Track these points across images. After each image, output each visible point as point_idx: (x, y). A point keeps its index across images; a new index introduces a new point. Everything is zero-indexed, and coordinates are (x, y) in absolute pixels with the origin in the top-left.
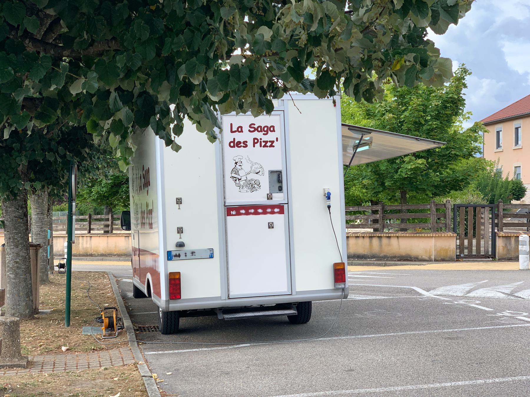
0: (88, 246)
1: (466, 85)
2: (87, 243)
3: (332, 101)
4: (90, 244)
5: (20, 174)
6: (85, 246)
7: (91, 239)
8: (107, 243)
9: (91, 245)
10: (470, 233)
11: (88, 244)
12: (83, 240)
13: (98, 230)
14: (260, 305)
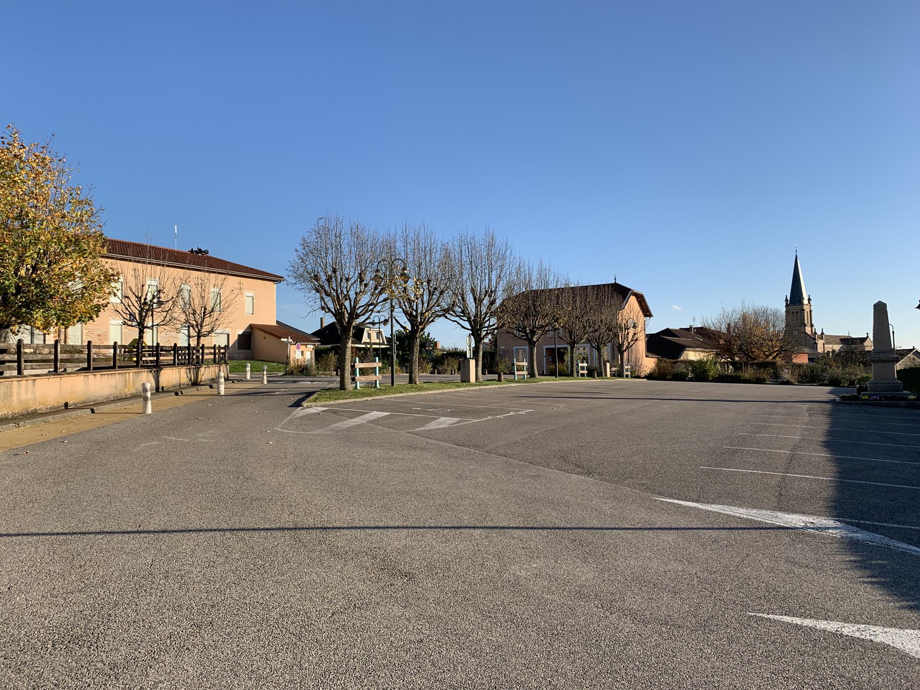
0: (30, 396)
1: (435, 340)
2: (27, 392)
3: (113, 311)
4: (32, 392)
5: (371, 337)
6: (23, 397)
7: (34, 385)
8: (60, 388)
9: (35, 394)
10: (348, 373)
11: (30, 392)
12: (19, 386)
13: (32, 369)
14: (846, 341)
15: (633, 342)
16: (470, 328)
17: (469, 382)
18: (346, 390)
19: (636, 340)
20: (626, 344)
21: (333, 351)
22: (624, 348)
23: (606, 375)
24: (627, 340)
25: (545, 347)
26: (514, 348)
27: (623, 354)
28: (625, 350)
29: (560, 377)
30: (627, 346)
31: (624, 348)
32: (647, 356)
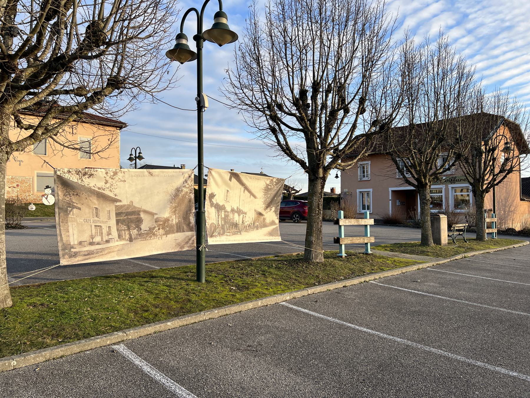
15: (504, 174)
16: (301, 128)
17: (374, 220)
18: (167, 54)
19: (510, 171)
20: (488, 178)
21: (278, 239)
22: (485, 187)
23: (438, 241)
24: (492, 170)
25: (391, 189)
26: (358, 191)
27: (482, 198)
28: (487, 191)
29: (467, 234)
30: (489, 183)
31: (485, 187)
32: (521, 200)
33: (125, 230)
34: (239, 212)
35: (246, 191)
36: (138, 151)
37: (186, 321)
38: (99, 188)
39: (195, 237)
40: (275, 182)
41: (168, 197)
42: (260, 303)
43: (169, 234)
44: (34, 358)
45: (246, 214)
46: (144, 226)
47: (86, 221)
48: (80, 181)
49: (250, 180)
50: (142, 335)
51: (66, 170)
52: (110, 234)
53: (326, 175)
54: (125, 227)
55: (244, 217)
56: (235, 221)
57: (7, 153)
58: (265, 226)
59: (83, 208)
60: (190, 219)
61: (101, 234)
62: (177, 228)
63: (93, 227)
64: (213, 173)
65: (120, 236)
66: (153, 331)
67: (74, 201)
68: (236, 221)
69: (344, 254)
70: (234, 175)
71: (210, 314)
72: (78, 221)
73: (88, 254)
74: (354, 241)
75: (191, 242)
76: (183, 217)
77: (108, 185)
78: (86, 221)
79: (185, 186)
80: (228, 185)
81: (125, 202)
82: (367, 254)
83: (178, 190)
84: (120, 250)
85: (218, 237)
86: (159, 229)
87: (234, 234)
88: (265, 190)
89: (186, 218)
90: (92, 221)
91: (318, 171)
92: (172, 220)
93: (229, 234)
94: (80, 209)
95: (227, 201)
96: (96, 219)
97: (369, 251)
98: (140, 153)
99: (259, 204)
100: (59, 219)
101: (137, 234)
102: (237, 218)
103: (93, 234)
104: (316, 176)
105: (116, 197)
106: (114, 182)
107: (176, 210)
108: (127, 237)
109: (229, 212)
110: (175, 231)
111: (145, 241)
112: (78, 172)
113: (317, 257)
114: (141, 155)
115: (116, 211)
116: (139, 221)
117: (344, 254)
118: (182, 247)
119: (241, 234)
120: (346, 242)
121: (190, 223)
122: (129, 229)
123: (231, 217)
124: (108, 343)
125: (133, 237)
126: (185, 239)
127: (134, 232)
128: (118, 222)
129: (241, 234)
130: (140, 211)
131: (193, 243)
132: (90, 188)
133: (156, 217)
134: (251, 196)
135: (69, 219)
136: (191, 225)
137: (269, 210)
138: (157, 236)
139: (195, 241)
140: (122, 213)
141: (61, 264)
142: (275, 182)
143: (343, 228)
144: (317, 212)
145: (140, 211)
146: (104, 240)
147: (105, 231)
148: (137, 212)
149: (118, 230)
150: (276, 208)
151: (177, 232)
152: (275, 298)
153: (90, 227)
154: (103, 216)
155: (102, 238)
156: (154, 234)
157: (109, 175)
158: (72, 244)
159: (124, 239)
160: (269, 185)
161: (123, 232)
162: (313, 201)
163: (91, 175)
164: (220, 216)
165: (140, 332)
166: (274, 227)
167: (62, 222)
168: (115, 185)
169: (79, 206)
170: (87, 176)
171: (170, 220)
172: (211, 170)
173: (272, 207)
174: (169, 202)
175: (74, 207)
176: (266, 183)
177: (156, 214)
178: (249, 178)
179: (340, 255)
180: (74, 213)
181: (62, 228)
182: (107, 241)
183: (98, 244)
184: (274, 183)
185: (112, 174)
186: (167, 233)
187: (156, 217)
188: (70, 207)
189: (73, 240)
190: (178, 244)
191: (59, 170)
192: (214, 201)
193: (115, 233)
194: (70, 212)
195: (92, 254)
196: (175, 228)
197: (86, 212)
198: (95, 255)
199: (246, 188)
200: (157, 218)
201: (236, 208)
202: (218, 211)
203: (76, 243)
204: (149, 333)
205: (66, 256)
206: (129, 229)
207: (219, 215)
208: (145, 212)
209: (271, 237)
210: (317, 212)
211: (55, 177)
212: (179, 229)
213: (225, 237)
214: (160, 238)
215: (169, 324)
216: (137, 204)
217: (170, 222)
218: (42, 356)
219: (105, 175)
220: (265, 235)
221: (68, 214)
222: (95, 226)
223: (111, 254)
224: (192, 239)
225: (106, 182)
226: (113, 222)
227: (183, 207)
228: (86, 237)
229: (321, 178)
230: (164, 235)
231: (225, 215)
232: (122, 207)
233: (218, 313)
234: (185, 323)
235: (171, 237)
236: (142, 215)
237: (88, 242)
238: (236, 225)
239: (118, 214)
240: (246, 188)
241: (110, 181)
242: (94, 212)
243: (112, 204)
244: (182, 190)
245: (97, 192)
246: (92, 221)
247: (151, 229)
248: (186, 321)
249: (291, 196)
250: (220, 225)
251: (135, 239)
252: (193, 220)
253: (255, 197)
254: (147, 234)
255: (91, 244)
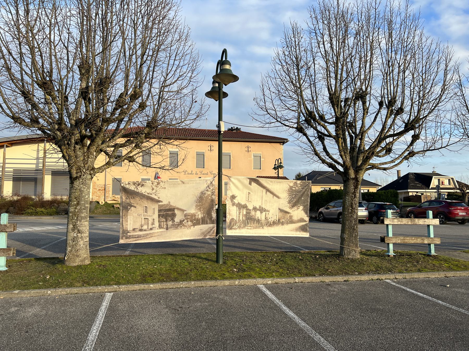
33: (163, 222)
34: (262, 210)
35: (268, 193)
36: (279, 162)
37: (166, 286)
38: (148, 194)
39: (215, 228)
40: (300, 184)
41: (195, 198)
42: (237, 283)
43: (196, 225)
44: (60, 292)
45: (268, 211)
46: (177, 220)
47: (139, 215)
48: (136, 189)
49: (271, 183)
50: (130, 290)
51: (127, 183)
52: (154, 224)
53: (358, 176)
54: (164, 220)
55: (267, 214)
56: (257, 218)
57: (91, 174)
58: (292, 222)
59: (137, 206)
60: (211, 215)
61: (148, 224)
62: (202, 221)
63: (143, 219)
64: (232, 179)
65: (160, 227)
66: (138, 288)
67: (132, 202)
68: (258, 217)
69: (392, 253)
70: (252, 180)
71: (186, 284)
72: (134, 215)
73: (138, 237)
74: (406, 241)
75: (212, 232)
76: (207, 213)
77: (154, 191)
78: (139, 215)
79: (207, 190)
80: (249, 189)
81: (165, 202)
82: (429, 255)
83: (203, 193)
84: (160, 235)
85: (238, 230)
86: (188, 221)
87: (256, 228)
88: (289, 191)
89: (209, 213)
90: (142, 215)
91: (348, 173)
92: (198, 215)
93: (250, 228)
94: (135, 207)
95: (248, 201)
96: (146, 214)
97: (433, 252)
98: (280, 163)
99: (284, 203)
100: (122, 213)
101: (171, 225)
102: (258, 215)
103: (143, 223)
104: (347, 177)
105: (159, 199)
106: (158, 189)
107: (201, 208)
108: (165, 226)
109: (250, 210)
110: (201, 224)
111: (177, 230)
112: (134, 184)
113: (349, 253)
114: (281, 164)
115: (158, 208)
116: (174, 215)
117: (392, 253)
118: (205, 236)
119: (263, 228)
120: (394, 241)
121: (212, 217)
122: (166, 221)
123: (253, 214)
124: (106, 291)
125: (169, 227)
126: (208, 230)
127: (170, 223)
128: (159, 216)
129: (263, 228)
130: (174, 209)
131: (213, 233)
132: (142, 194)
133: (185, 212)
134: (274, 197)
135: (129, 214)
136: (213, 219)
137: (296, 209)
138: (186, 227)
139: (215, 231)
140: (162, 210)
141: (119, 243)
142: (300, 184)
143: (390, 228)
144: (350, 211)
145: (174, 209)
146: (149, 228)
147: (150, 222)
148: (172, 210)
149: (159, 221)
150: (304, 207)
151: (202, 224)
152: (255, 280)
153: (141, 219)
154: (150, 212)
155: (148, 227)
156: (184, 225)
157: (154, 184)
158: (129, 230)
159: (162, 228)
160: (293, 187)
161: (163, 223)
162: (346, 200)
163: (143, 185)
164: (241, 213)
165: (129, 288)
166: (304, 223)
167: (124, 216)
168: (159, 191)
169: (135, 205)
170: (140, 186)
171: (196, 215)
172: (230, 177)
173: (300, 206)
174: (195, 202)
175: (131, 206)
176: (289, 186)
177: (186, 211)
178: (270, 182)
179: (388, 254)
180: (132, 209)
181: (123, 220)
182: (151, 229)
183: (145, 230)
184: (299, 185)
185: (156, 184)
186: (194, 225)
187: (185, 212)
188: (129, 206)
189: (130, 228)
190: (203, 233)
191: (123, 183)
192: (236, 201)
193: (157, 224)
194: (129, 209)
195: (140, 237)
196: (201, 221)
197: (140, 209)
198: (141, 238)
199: (268, 190)
200: (186, 214)
201: (258, 207)
202: (240, 209)
203: (131, 229)
204: (135, 289)
205: (124, 238)
206: (166, 221)
207: (240, 213)
208: (178, 209)
209: (298, 233)
210: (350, 211)
211: (121, 188)
212: (203, 221)
213: (246, 230)
214: (189, 228)
215: (152, 286)
216: (173, 204)
217: (197, 217)
218: (65, 291)
219: (152, 185)
220: (292, 231)
221: (128, 211)
222: (145, 218)
223: (152, 238)
224: (213, 230)
225: (153, 189)
226: (156, 216)
227: (207, 205)
228: (138, 226)
229: (353, 179)
230: (192, 226)
231: (246, 212)
232: (162, 206)
233: (195, 284)
234: (165, 287)
235: (198, 227)
236: (176, 211)
237: (139, 229)
238: (258, 221)
239: (160, 211)
240: (268, 190)
241: (155, 188)
242: (145, 209)
243: (156, 204)
244: (205, 193)
245: (147, 196)
246: (142, 215)
247: (181, 222)
248: (166, 286)
249: (465, 195)
250: (241, 220)
251: (170, 228)
252: (214, 215)
253: (278, 197)
254: (178, 225)
255: (141, 230)
